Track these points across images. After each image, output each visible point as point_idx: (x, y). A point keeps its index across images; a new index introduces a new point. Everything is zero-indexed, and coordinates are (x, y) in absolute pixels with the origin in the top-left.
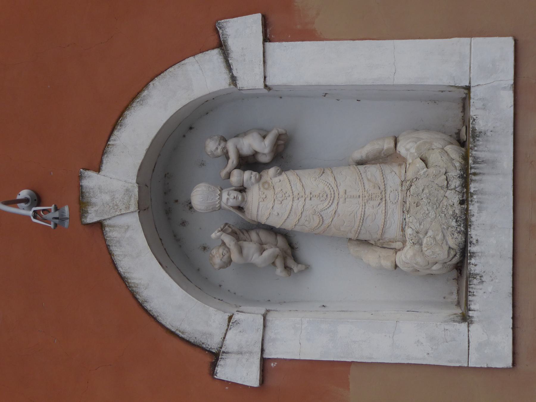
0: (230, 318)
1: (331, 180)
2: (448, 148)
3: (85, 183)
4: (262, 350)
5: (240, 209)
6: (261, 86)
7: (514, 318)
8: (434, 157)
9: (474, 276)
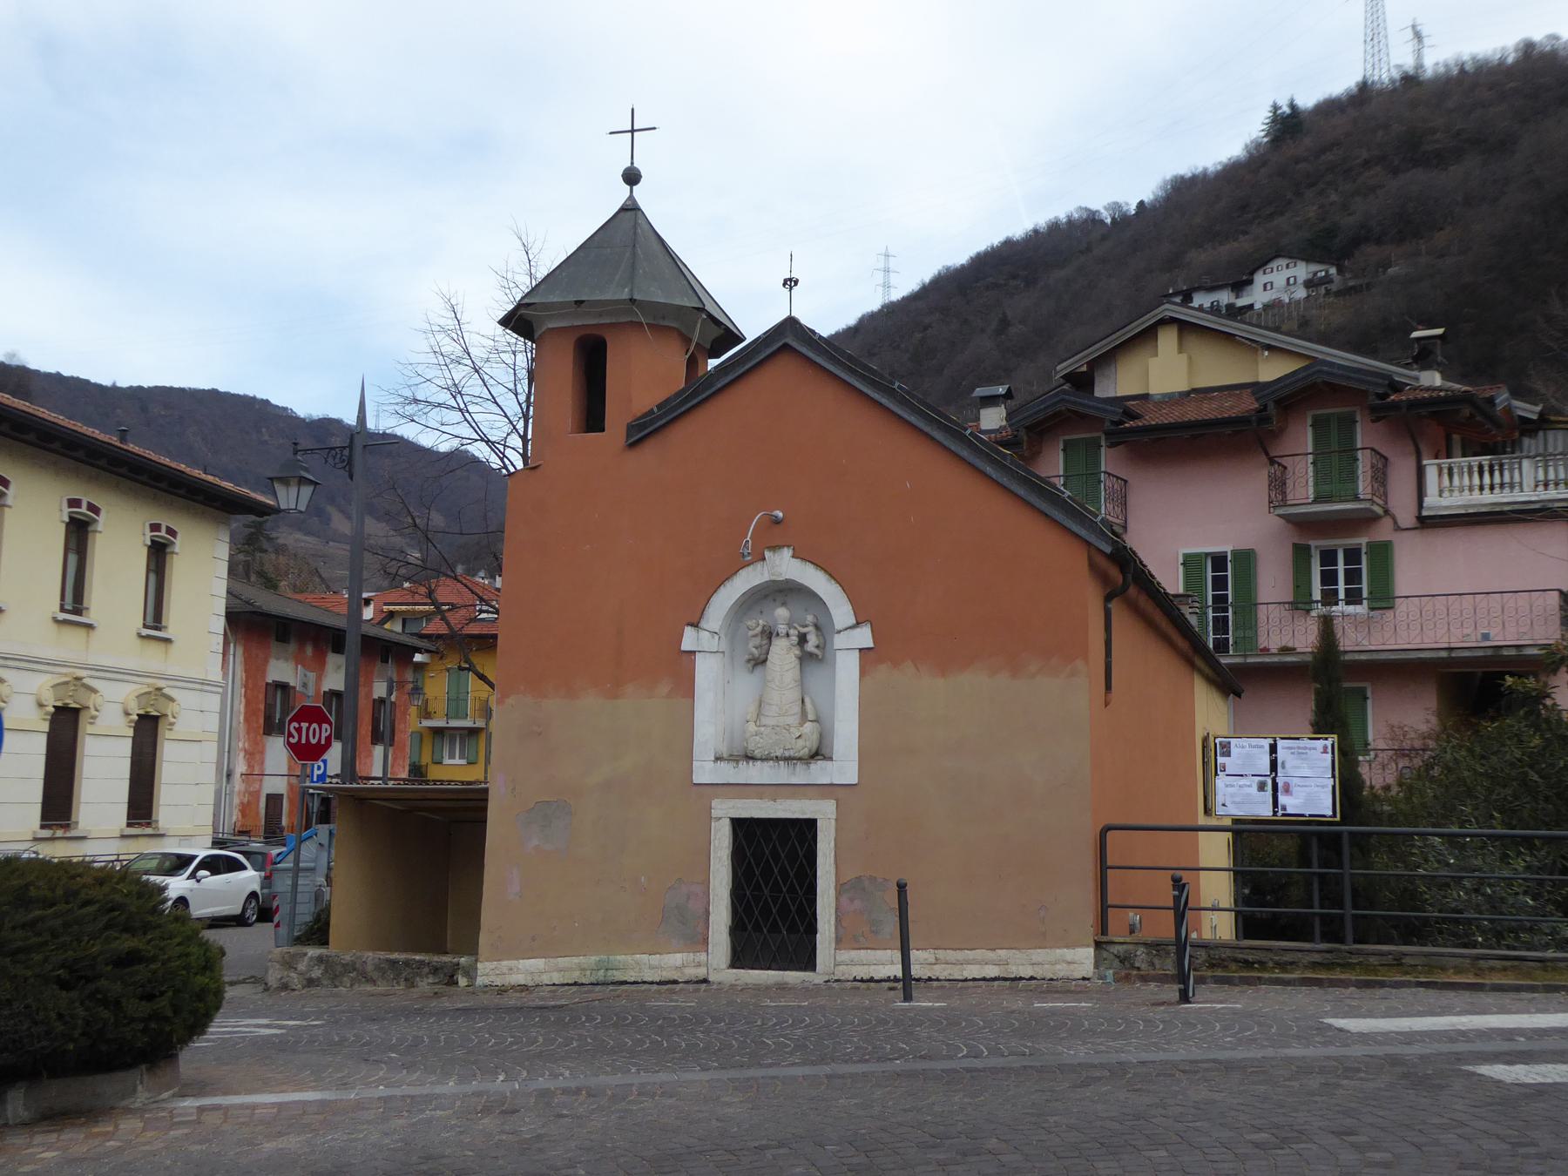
0: (716, 633)
1: (791, 686)
2: (806, 750)
3: (786, 549)
4: (699, 651)
5: (778, 634)
6: (835, 648)
7: (717, 784)
8: (801, 742)
9: (737, 764)
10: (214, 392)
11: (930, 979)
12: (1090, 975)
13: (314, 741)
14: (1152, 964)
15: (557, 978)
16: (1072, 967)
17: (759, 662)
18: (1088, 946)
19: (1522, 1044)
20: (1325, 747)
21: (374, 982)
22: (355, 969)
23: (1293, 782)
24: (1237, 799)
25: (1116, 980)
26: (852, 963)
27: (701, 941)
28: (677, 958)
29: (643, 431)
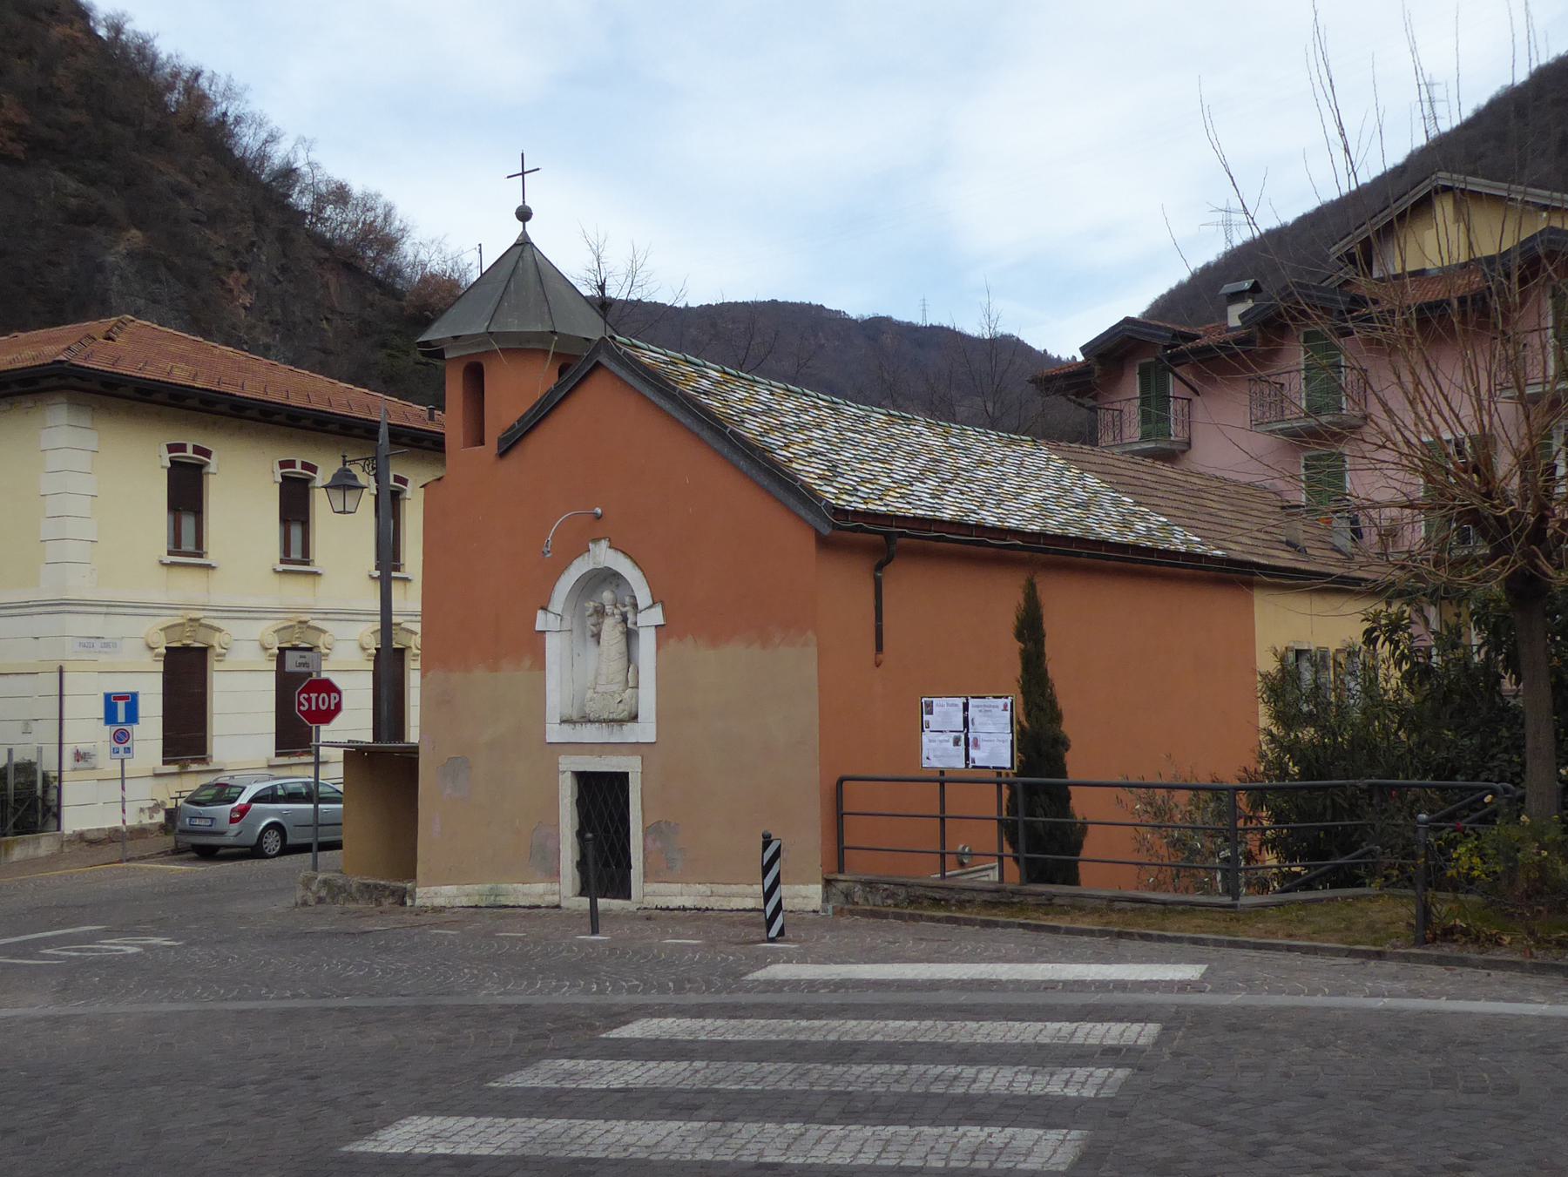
2: (626, 713)
8: (621, 706)
10: (774, 302)
11: (707, 909)
12: (818, 908)
13: (324, 708)
14: (867, 899)
15: (465, 901)
16: (805, 901)
17: (597, 637)
18: (818, 883)
19: (824, 997)
20: (1005, 706)
21: (355, 900)
22: (345, 891)
23: (981, 737)
24: (938, 753)
25: (834, 914)
26: (654, 894)
27: (554, 874)
28: (540, 887)
29: (510, 444)
